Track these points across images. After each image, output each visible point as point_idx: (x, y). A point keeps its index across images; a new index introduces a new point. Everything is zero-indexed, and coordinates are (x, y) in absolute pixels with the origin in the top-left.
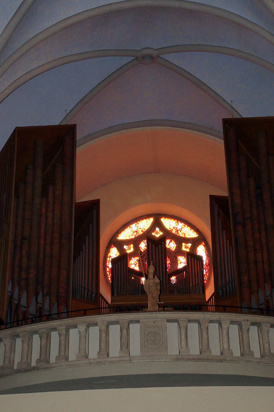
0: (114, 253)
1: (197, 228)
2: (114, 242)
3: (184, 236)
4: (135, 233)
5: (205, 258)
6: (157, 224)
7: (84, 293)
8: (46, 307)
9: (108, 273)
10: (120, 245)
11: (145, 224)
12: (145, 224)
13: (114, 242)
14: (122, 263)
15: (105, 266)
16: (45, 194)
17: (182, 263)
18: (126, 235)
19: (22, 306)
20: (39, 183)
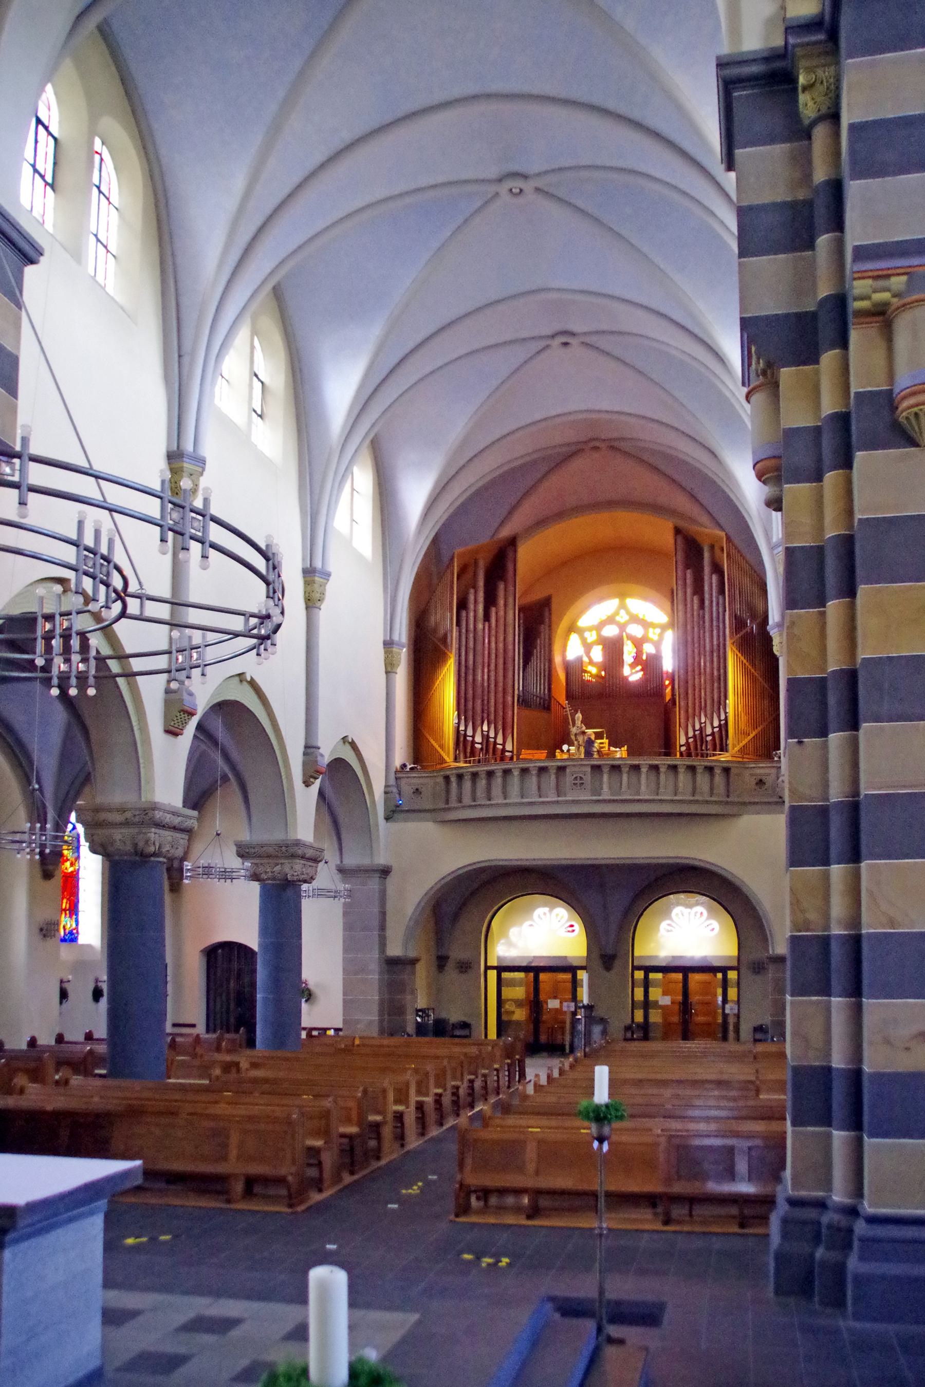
8: (492, 734)
16: (487, 617)
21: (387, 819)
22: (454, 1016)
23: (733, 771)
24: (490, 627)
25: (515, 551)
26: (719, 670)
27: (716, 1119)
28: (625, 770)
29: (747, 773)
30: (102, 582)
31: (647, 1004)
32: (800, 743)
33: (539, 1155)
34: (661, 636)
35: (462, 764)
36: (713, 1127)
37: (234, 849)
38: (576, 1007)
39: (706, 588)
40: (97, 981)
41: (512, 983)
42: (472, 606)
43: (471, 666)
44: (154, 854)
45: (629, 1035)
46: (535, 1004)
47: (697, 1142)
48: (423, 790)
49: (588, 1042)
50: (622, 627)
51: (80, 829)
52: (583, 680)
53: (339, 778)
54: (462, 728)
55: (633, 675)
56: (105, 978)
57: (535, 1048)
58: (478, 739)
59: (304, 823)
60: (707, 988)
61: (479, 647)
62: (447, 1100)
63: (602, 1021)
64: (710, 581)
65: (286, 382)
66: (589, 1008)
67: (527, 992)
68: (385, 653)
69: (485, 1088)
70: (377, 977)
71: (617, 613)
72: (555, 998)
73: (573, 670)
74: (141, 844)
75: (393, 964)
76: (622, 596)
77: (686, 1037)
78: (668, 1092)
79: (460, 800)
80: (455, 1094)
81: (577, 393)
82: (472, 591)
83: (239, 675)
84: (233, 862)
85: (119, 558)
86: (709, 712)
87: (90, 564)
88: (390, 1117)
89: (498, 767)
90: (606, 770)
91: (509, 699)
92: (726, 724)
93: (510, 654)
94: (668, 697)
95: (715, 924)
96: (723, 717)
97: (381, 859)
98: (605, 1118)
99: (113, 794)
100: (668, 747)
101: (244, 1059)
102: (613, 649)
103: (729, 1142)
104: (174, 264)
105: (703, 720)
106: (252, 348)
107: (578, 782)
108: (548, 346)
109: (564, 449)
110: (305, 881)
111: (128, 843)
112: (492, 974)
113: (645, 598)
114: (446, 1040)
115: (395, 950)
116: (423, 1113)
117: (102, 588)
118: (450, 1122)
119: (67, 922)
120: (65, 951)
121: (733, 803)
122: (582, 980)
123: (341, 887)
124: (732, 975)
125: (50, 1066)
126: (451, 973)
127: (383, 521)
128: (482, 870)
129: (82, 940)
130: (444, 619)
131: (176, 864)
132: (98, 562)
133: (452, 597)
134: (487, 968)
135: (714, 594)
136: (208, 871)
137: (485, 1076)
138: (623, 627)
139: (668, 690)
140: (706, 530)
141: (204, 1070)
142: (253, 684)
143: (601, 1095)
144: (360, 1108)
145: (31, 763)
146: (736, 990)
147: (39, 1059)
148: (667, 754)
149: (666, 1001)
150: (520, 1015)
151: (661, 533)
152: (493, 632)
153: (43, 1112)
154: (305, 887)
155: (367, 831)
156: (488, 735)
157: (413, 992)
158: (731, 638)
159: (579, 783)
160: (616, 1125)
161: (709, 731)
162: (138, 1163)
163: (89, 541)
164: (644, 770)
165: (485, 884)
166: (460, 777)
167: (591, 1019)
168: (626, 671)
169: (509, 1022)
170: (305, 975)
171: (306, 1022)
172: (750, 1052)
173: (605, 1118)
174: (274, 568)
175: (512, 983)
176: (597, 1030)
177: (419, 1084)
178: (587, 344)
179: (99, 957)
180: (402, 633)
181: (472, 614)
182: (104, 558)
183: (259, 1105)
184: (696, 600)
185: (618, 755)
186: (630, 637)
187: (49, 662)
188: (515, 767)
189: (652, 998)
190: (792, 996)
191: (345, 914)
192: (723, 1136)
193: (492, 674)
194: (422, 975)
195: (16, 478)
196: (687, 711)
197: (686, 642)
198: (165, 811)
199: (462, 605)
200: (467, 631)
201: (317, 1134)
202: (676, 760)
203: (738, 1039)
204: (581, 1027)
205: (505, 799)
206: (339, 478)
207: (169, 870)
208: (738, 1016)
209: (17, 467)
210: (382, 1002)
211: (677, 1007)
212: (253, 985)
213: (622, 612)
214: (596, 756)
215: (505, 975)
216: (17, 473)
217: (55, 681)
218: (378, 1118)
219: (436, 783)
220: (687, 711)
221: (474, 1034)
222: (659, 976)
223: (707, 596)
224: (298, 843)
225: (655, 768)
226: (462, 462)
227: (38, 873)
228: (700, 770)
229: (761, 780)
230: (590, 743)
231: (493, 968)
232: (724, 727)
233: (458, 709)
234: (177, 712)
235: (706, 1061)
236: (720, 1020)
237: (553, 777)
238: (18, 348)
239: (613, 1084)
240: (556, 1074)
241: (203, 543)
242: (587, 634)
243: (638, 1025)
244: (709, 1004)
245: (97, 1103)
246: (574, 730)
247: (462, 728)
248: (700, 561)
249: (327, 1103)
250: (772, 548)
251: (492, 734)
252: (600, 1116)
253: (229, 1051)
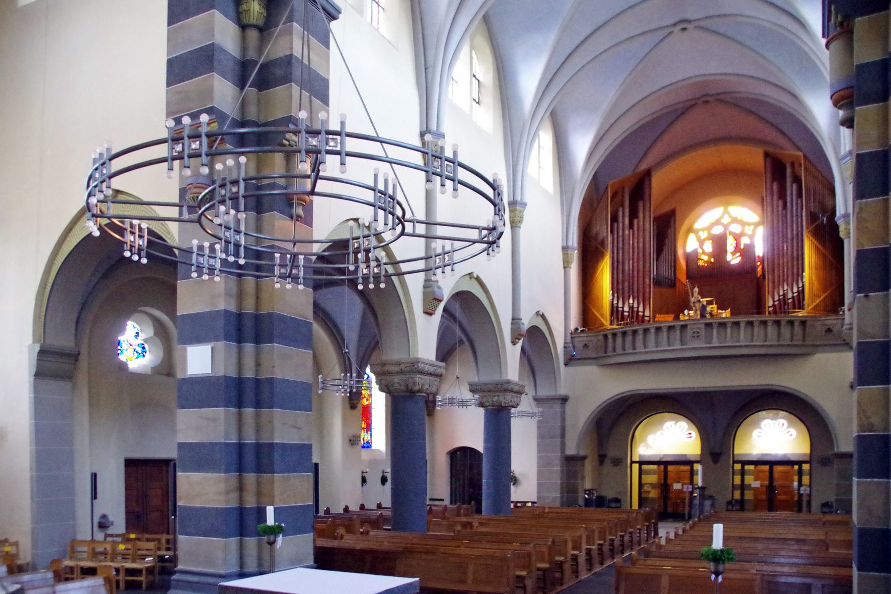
8: (636, 306)
16: (631, 226)
21: (566, 364)
22: (609, 494)
23: (808, 323)
25: (650, 180)
26: (798, 250)
27: (795, 564)
28: (729, 325)
30: (390, 213)
31: (743, 487)
32: (866, 296)
33: (670, 584)
34: (754, 231)
35: (615, 327)
36: (794, 570)
37: (468, 387)
38: (693, 488)
39: (788, 193)
40: (383, 472)
41: (649, 473)
42: (621, 219)
43: (621, 260)
44: (419, 391)
45: (730, 508)
46: (664, 487)
47: (783, 580)
48: (590, 345)
49: (701, 511)
50: (726, 227)
51: (373, 377)
52: (698, 266)
53: (534, 339)
54: (615, 302)
55: (734, 260)
56: (389, 470)
57: (666, 515)
58: (626, 309)
59: (512, 367)
60: (787, 476)
61: (626, 247)
62: (606, 548)
63: (711, 497)
64: (791, 189)
65: (494, 77)
66: (702, 489)
67: (659, 479)
69: (631, 541)
70: (559, 468)
71: (722, 217)
72: (678, 482)
73: (691, 259)
74: (410, 385)
75: (569, 460)
76: (726, 204)
77: (771, 509)
78: (760, 546)
79: (614, 350)
80: (612, 545)
81: (691, 63)
82: (621, 209)
83: (469, 274)
84: (467, 395)
85: (400, 197)
87: (382, 201)
88: (569, 557)
89: (640, 327)
90: (715, 326)
91: (647, 281)
92: (803, 290)
93: (648, 251)
94: (759, 274)
95: (793, 431)
96: (800, 285)
97: (562, 391)
98: (720, 559)
99: (393, 354)
100: (759, 306)
101: (475, 520)
102: (720, 243)
103: (808, 580)
104: (420, 8)
105: (785, 288)
106: (471, 58)
107: (696, 335)
108: (671, 33)
109: (680, 106)
110: (513, 407)
111: (403, 384)
112: (636, 467)
113: (743, 206)
114: (605, 509)
115: (571, 451)
116: (591, 556)
117: (390, 216)
118: (608, 563)
119: (364, 436)
120: (365, 454)
121: (807, 346)
122: (697, 470)
123: (536, 410)
124: (806, 467)
125: (357, 525)
126: (608, 467)
127: (560, 166)
128: (631, 397)
129: (374, 447)
130: (603, 229)
131: (431, 398)
132: (386, 201)
133: (607, 215)
134: (632, 462)
135: (794, 198)
136: (451, 401)
137: (631, 533)
138: (729, 226)
139: (759, 269)
140: (789, 152)
141: (450, 527)
142: (478, 279)
143: (718, 543)
144: (550, 554)
145: (344, 341)
146: (808, 477)
147: (350, 519)
148: (759, 313)
149: (756, 484)
150: (654, 494)
151: (754, 158)
152: (636, 236)
153: (355, 550)
154: (513, 410)
155: (553, 373)
156: (633, 307)
157: (583, 478)
158: (807, 228)
159: (696, 336)
160: (728, 565)
161: (790, 295)
162: (417, 579)
163: (381, 187)
164: (742, 325)
165: (630, 407)
166: (614, 335)
167: (703, 497)
168: (729, 257)
169: (646, 499)
170: (513, 467)
171: (513, 498)
172: (820, 520)
173: (720, 559)
174: (499, 195)
175: (649, 473)
176: (708, 503)
177: (588, 537)
178: (702, 28)
179: (384, 457)
180: (574, 240)
181: (621, 225)
182: (390, 197)
183: (485, 549)
184: (780, 203)
185: (724, 316)
186: (731, 233)
187: (357, 268)
188: (652, 326)
189: (746, 482)
190: (859, 477)
191: (539, 427)
192: (804, 577)
193: (636, 264)
194: (589, 467)
195: (338, 148)
196: (774, 282)
197: (773, 235)
198: (424, 363)
199: (614, 219)
201: (524, 568)
202: (766, 317)
203: (810, 511)
204: (697, 502)
205: (645, 348)
206: (531, 138)
207: (426, 402)
208: (810, 495)
209: (339, 141)
210: (562, 484)
211: (764, 489)
212: (480, 474)
213: (726, 216)
214: (708, 316)
215: (644, 467)
216: (339, 145)
217: (360, 280)
218: (562, 558)
219: (598, 340)
220: (774, 282)
221: (623, 507)
222: (752, 467)
223: (789, 199)
224: (508, 382)
225: (751, 323)
226: (612, 121)
227: (348, 406)
228: (783, 323)
230: (704, 308)
231: (636, 462)
232: (801, 292)
233: (613, 290)
234: (431, 300)
235: (785, 525)
236: (796, 498)
237: (678, 332)
238: (328, 74)
239: (726, 539)
240: (680, 532)
241: (453, 180)
242: (701, 233)
243: (737, 501)
244: (788, 489)
245: (386, 546)
246: (693, 300)
247: (615, 302)
248: (786, 173)
249: (529, 548)
250: (840, 160)
251: (636, 306)
252: (717, 557)
253: (465, 515)
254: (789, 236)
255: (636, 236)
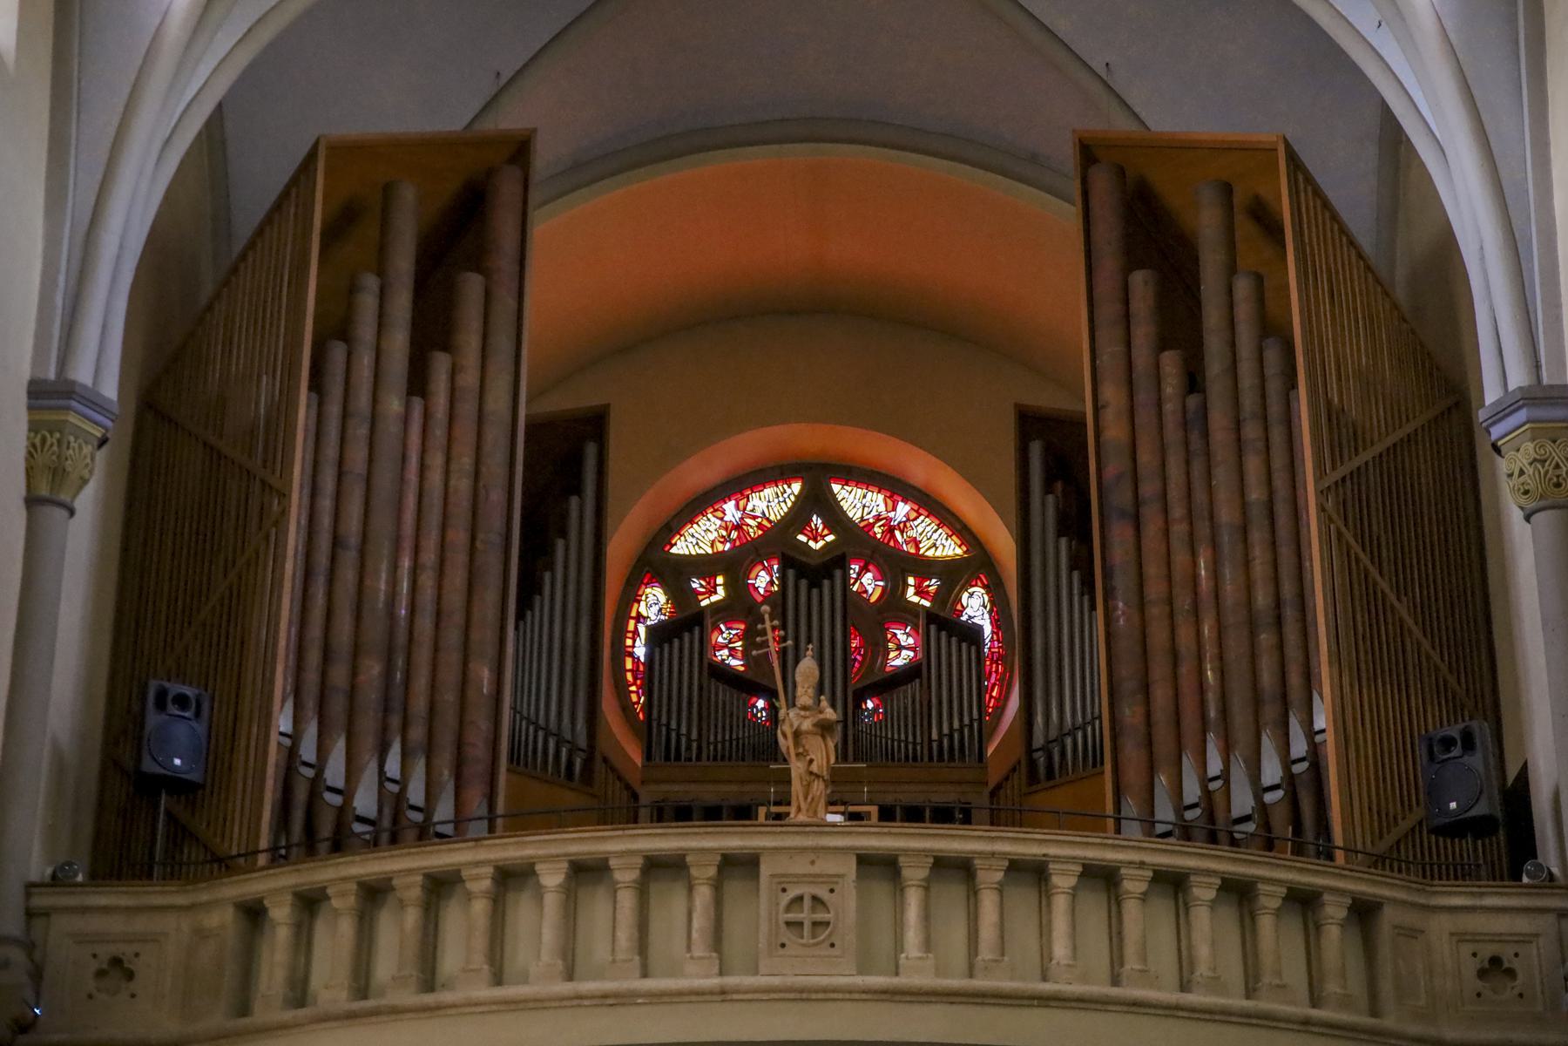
0: (654, 603)
1: (772, 468)
2: (655, 564)
3: (913, 551)
4: (734, 535)
5: (988, 630)
6: (818, 501)
7: (535, 742)
8: (416, 794)
9: (629, 676)
10: (674, 575)
11: (771, 503)
12: (771, 503)
13: (655, 564)
14: (687, 645)
15: (621, 652)
16: (418, 383)
17: (903, 649)
18: (699, 538)
19: (413, 808)
20: (399, 342)
24: (427, 415)
29: (1439, 928)
39: (1212, 317)
42: (366, 331)
68: (34, 427)
82: (371, 282)
86: (1242, 734)
96: (1299, 747)
105: (1215, 766)
107: (805, 915)
152: (439, 432)
156: (400, 797)
181: (365, 360)
184: (1171, 362)
193: (427, 581)
196: (1149, 743)
200: (345, 415)
205: (498, 980)
223: (1214, 345)
229: (1495, 961)
254: (1227, 514)
255: (439, 432)
